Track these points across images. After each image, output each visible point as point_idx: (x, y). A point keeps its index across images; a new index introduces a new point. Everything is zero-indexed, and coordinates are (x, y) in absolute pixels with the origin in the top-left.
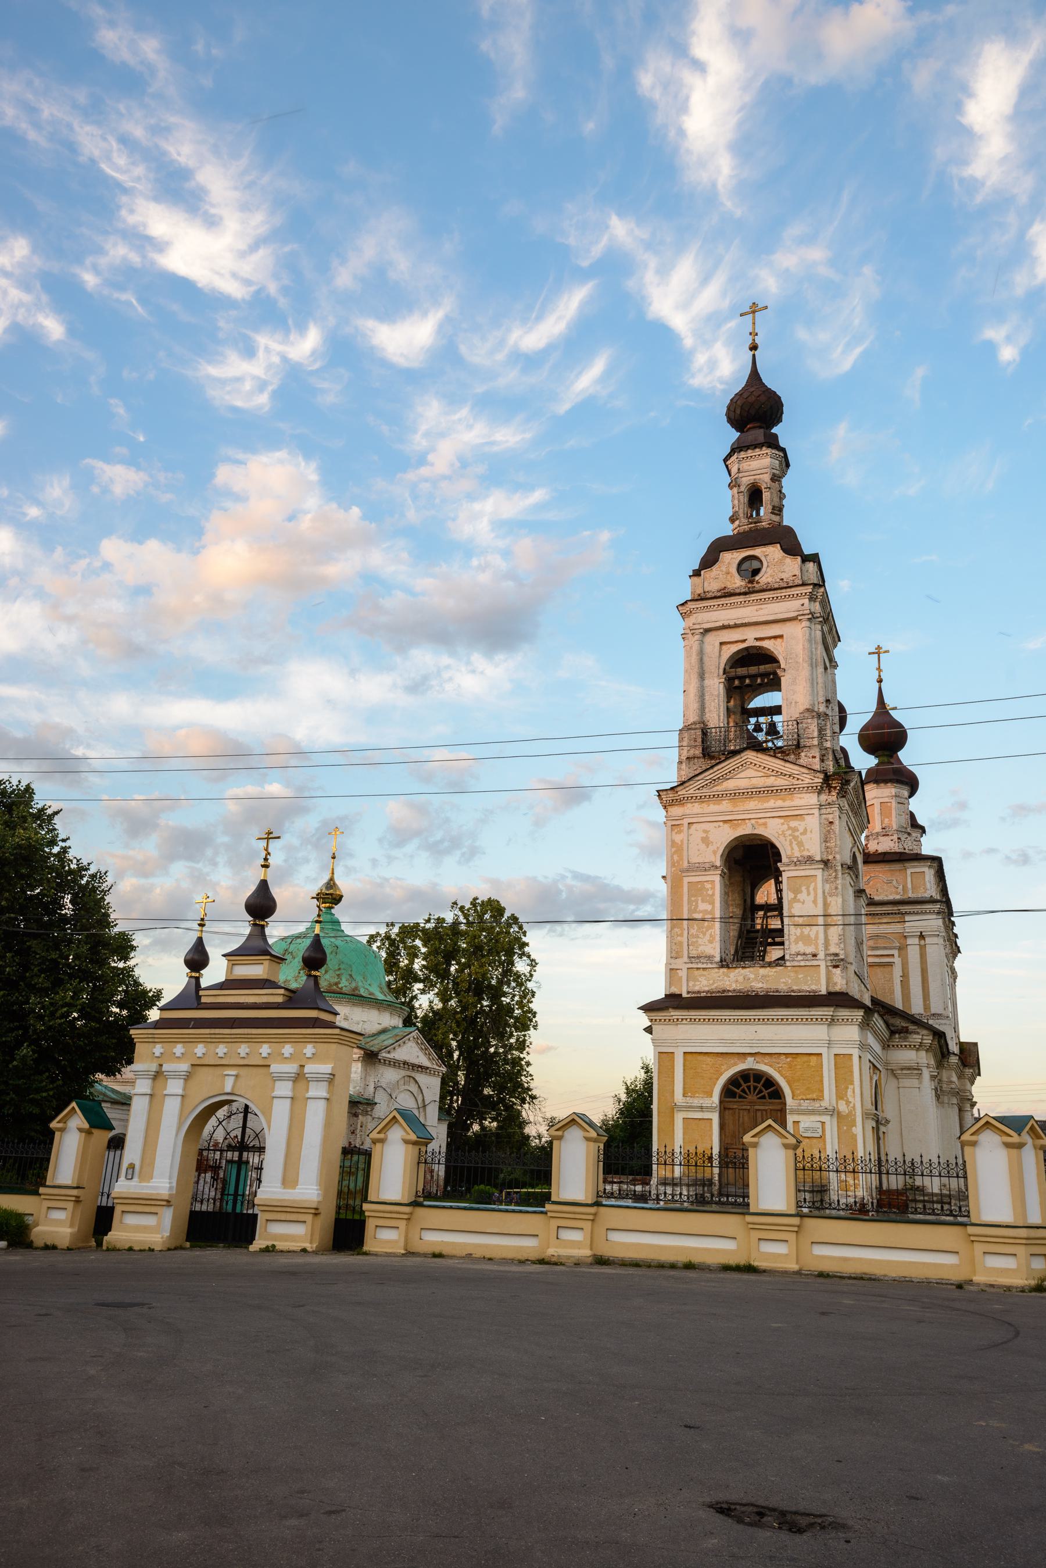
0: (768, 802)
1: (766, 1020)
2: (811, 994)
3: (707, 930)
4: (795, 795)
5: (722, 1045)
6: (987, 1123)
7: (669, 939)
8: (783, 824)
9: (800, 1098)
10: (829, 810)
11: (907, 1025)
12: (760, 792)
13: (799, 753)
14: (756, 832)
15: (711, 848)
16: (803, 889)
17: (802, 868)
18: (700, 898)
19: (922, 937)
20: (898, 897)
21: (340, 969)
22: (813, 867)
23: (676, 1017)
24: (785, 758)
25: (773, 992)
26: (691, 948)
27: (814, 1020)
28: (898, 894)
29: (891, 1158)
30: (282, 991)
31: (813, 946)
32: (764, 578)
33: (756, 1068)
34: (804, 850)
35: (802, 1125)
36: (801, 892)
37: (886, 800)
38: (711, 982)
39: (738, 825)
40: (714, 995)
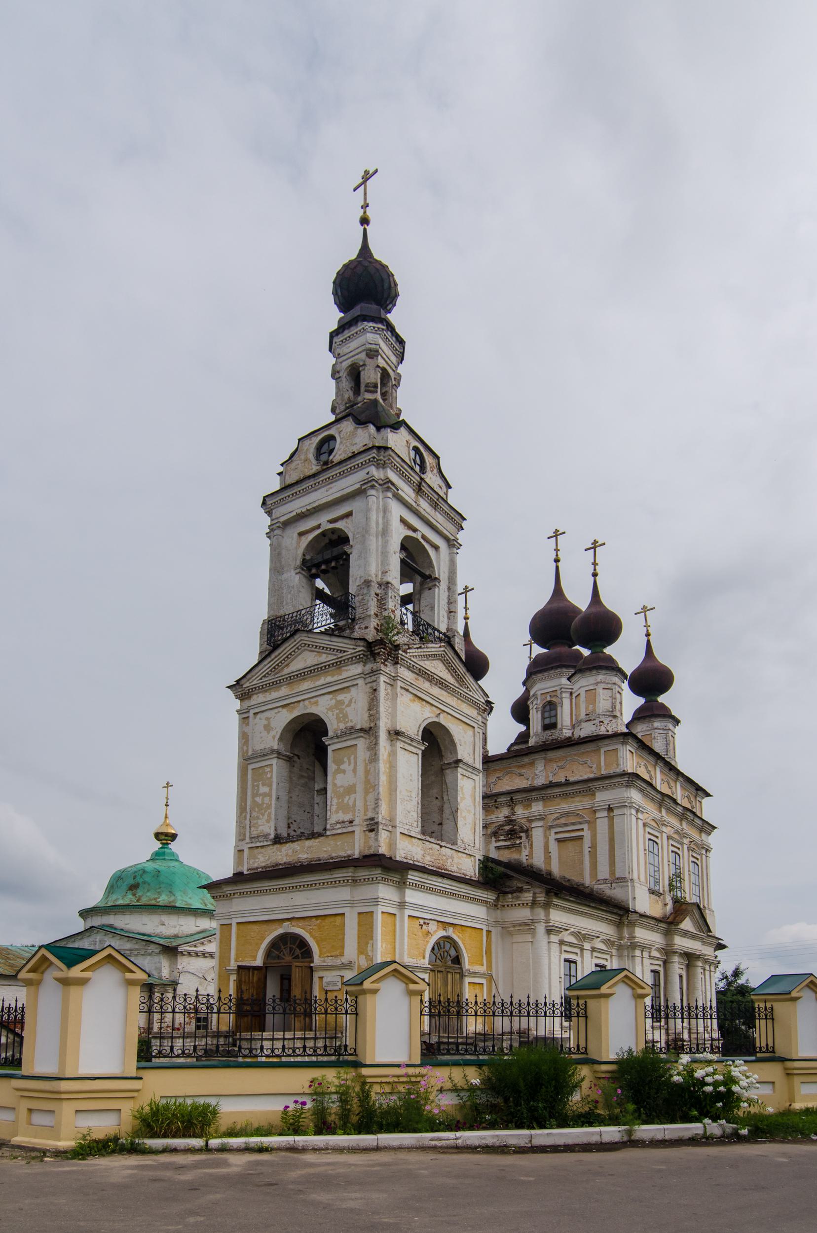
0: (319, 680)
1: (298, 887)
2: (346, 859)
3: (265, 811)
4: (343, 668)
5: (265, 913)
6: (110, 956)
7: (238, 824)
8: (331, 699)
9: (326, 955)
10: (373, 678)
11: (522, 885)
12: (311, 671)
13: (354, 626)
14: (308, 711)
15: (273, 733)
16: (345, 759)
17: (343, 739)
18: (260, 783)
19: (610, 809)
20: (592, 776)
21: (160, 888)
22: (353, 736)
23: (228, 892)
24: (342, 634)
25: (316, 861)
26: (252, 829)
27: (338, 882)
28: (592, 772)
29: (700, 1004)
30: (317, 630)
31: (351, 813)
32: (337, 456)
33: (291, 931)
34: (348, 722)
35: (325, 980)
36: (343, 763)
37: (591, 687)
38: (267, 858)
39: (294, 708)
40: (268, 869)
